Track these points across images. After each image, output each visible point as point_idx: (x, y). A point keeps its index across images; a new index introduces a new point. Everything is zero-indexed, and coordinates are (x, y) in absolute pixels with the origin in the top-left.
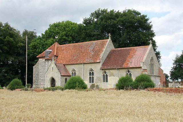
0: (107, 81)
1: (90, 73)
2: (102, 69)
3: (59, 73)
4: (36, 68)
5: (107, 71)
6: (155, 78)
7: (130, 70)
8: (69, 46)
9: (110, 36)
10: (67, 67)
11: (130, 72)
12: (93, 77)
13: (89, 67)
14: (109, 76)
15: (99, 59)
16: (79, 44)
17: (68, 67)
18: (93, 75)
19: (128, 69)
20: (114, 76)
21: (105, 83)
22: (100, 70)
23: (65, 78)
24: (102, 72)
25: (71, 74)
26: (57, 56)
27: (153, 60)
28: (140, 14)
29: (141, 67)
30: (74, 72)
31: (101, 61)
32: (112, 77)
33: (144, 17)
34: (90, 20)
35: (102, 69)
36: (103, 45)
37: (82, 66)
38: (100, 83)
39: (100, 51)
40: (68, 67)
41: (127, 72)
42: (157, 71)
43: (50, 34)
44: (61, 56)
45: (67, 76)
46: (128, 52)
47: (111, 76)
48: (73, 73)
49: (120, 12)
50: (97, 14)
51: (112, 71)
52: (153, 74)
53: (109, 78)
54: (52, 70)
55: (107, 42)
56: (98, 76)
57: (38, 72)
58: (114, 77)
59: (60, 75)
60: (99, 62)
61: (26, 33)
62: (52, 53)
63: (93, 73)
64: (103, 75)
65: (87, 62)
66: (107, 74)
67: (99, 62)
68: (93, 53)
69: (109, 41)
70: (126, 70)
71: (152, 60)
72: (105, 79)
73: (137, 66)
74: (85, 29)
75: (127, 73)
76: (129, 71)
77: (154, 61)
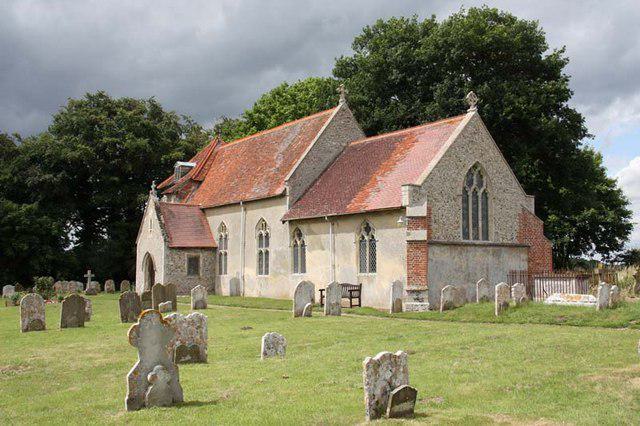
0: (373, 268)
6: (497, 255)
12: (267, 252)
23: (186, 255)
45: (197, 248)
50: (367, 38)
61: (63, 128)
70: (357, 223)
72: (299, 263)
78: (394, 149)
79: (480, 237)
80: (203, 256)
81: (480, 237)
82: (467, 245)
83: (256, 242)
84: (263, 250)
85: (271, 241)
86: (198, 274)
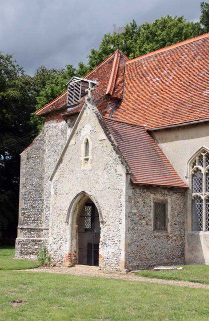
54: (83, 158)
57: (42, 178)
80: (172, 201)
86: (166, 229)
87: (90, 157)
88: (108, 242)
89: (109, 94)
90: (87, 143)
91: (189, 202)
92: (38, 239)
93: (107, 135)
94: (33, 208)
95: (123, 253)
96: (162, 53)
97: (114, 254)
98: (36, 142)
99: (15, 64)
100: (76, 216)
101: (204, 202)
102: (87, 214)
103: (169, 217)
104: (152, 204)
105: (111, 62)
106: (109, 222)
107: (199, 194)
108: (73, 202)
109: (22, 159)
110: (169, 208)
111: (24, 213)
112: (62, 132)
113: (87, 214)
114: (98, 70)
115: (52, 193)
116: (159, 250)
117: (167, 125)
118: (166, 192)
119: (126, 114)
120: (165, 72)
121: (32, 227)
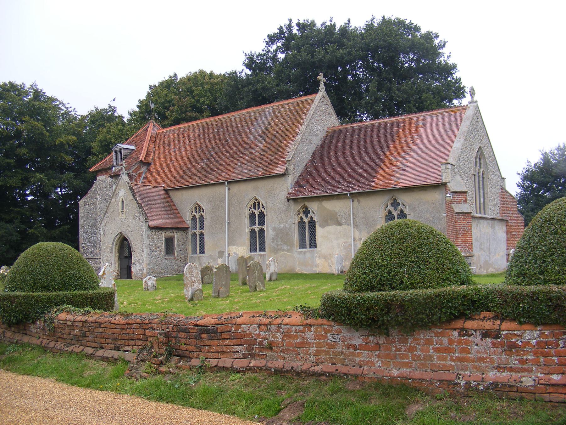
0: (313, 244)
1: (252, 215)
2: (295, 200)
3: (142, 219)
4: (87, 206)
5: (313, 206)
6: (493, 228)
7: (403, 198)
8: (187, 129)
9: (322, 84)
10: (172, 197)
11: (401, 207)
12: (262, 231)
13: (248, 192)
14: (322, 226)
15: (284, 163)
16: (219, 121)
17: (180, 198)
18: (262, 222)
19: (394, 192)
20: (340, 224)
21: (308, 249)
22: (286, 203)
23: (163, 235)
24: (295, 208)
25: (189, 223)
26: (149, 164)
27: (482, 161)
28: (417, 29)
29: (444, 185)
30: (198, 216)
31: (291, 169)
32: (332, 228)
33: (429, 37)
34: (264, 57)
35: (295, 200)
36: (297, 116)
37: (225, 190)
38: (288, 251)
39: (288, 133)
40: (180, 198)
41: (390, 207)
42: (498, 200)
43: (144, 113)
44: (160, 161)
46: (391, 134)
47: (328, 225)
48: (194, 219)
49: (353, 25)
51: (329, 205)
52: (485, 213)
53: (320, 231)
54: (120, 211)
55: (312, 101)
56: (282, 226)
57: (96, 220)
58: (339, 227)
59: (144, 228)
60: (283, 175)
62: (134, 155)
63: (262, 215)
64: (297, 220)
65: (240, 177)
66: (312, 218)
67: (283, 175)
68: (261, 145)
69: (320, 98)
71: (480, 159)
72: (308, 236)
73: (429, 182)
74: (248, 81)
75: (390, 212)
76: (395, 204)
77: (486, 166)
78: (396, 133)
79: (198, 228)
80: (177, 236)
81: (198, 228)
82: (481, 218)
83: (247, 221)
84: (257, 228)
85: (268, 219)
86: (174, 254)
87: (125, 210)
88: (136, 263)
89: (141, 160)
90: (123, 201)
91: (190, 237)
92: (96, 266)
93: (134, 197)
94: (90, 243)
95: (145, 269)
96: (181, 128)
97: (141, 270)
98: (91, 193)
99: (68, 106)
100: (117, 248)
101: (198, 236)
102: (124, 248)
103: (176, 246)
104: (164, 239)
105: (146, 130)
106: (137, 251)
107: (195, 231)
108: (114, 239)
109: (80, 206)
110: (176, 241)
111: (83, 247)
112: (110, 185)
113: (124, 248)
114: (137, 136)
115: (102, 233)
116: (169, 267)
117: (176, 186)
118: (174, 231)
119: (153, 176)
120: (181, 144)
121: (90, 257)
